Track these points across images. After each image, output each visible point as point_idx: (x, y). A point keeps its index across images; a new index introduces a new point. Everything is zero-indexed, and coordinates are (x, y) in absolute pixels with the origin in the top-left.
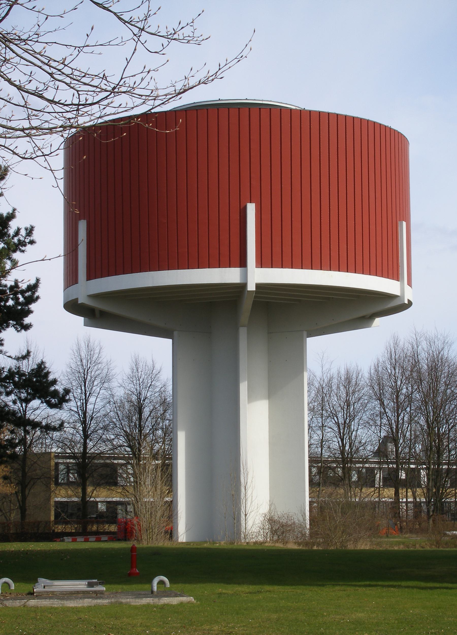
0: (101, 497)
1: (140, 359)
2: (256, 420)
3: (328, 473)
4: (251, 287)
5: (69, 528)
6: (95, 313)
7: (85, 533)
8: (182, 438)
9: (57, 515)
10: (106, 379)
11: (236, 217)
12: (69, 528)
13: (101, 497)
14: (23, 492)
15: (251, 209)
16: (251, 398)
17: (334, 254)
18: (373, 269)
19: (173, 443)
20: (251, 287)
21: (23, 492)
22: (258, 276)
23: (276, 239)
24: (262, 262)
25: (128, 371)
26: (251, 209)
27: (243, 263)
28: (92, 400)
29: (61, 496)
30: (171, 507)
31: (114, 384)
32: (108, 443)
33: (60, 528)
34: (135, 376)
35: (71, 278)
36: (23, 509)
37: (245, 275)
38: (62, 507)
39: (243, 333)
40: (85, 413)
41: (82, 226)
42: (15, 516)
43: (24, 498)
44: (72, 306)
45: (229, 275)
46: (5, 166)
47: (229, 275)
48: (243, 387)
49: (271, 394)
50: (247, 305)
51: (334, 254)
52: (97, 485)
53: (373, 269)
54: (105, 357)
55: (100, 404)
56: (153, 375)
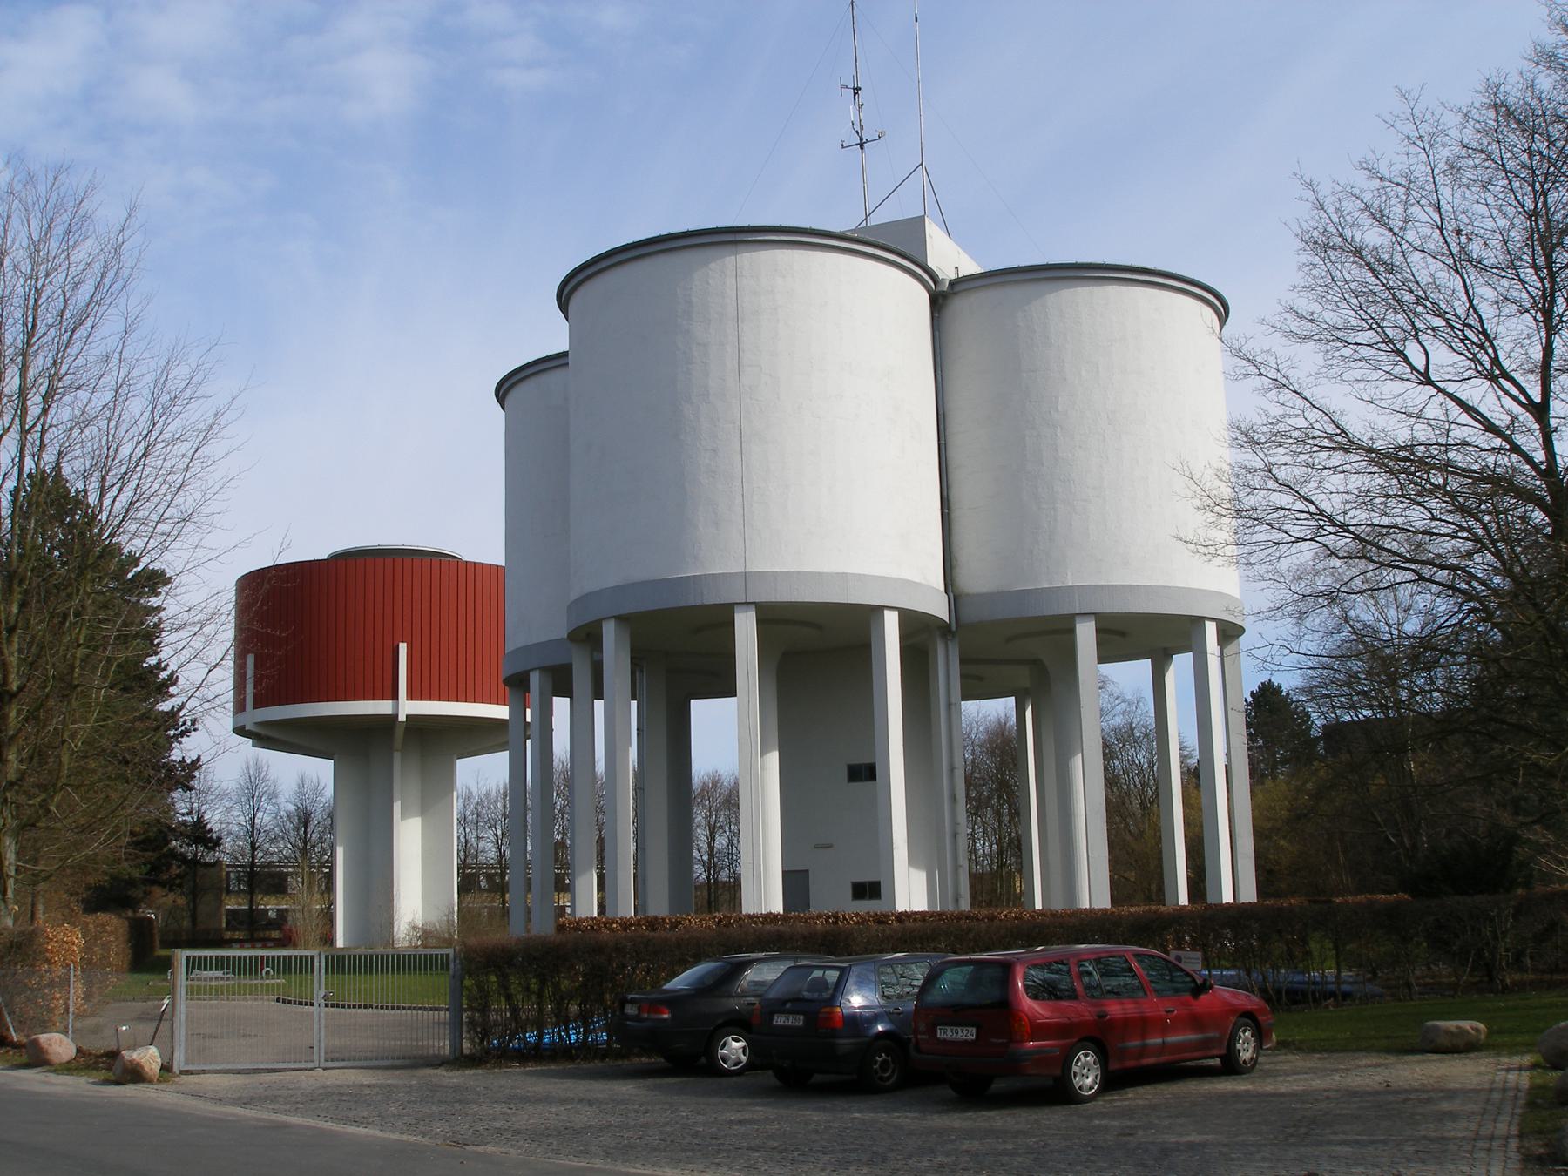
0: (270, 905)
1: (304, 776)
2: (409, 836)
3: (473, 878)
4: (402, 718)
5: (237, 935)
6: (267, 737)
7: (252, 941)
8: (340, 853)
9: (228, 923)
10: (273, 795)
11: (388, 656)
12: (237, 935)
13: (270, 905)
14: (194, 901)
15: (403, 647)
16: (404, 816)
17: (478, 689)
18: (479, 572)
19: (333, 856)
20: (402, 718)
21: (194, 901)
22: (408, 708)
23: (426, 674)
24: (412, 696)
25: (295, 787)
26: (403, 647)
27: (395, 697)
28: (260, 815)
29: (231, 904)
30: (328, 916)
31: (281, 799)
32: (276, 851)
33: (228, 935)
34: (301, 790)
35: (240, 707)
36: (194, 918)
37: (396, 707)
38: (232, 914)
39: (397, 756)
40: (253, 826)
41: (251, 659)
42: (186, 923)
43: (195, 908)
44: (240, 731)
45: (383, 707)
46: (159, 609)
47: (383, 707)
48: (397, 807)
49: (424, 811)
50: (399, 733)
51: (478, 689)
52: (267, 892)
53: (479, 572)
54: (272, 774)
55: (267, 819)
56: (318, 791)
